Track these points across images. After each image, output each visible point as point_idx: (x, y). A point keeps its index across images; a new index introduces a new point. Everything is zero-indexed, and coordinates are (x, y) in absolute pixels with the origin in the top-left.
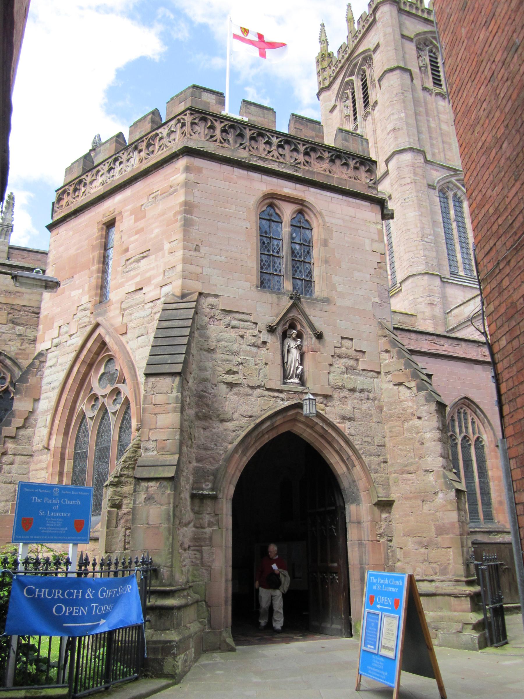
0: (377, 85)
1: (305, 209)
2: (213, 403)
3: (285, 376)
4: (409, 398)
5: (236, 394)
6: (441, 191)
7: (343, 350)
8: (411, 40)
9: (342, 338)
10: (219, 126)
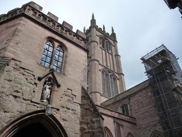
0: (89, 45)
1: (62, 46)
2: (3, 103)
3: (42, 98)
4: (90, 115)
5: (16, 101)
6: (102, 72)
7: (67, 93)
8: (98, 36)
9: (68, 89)
10: (38, 13)
